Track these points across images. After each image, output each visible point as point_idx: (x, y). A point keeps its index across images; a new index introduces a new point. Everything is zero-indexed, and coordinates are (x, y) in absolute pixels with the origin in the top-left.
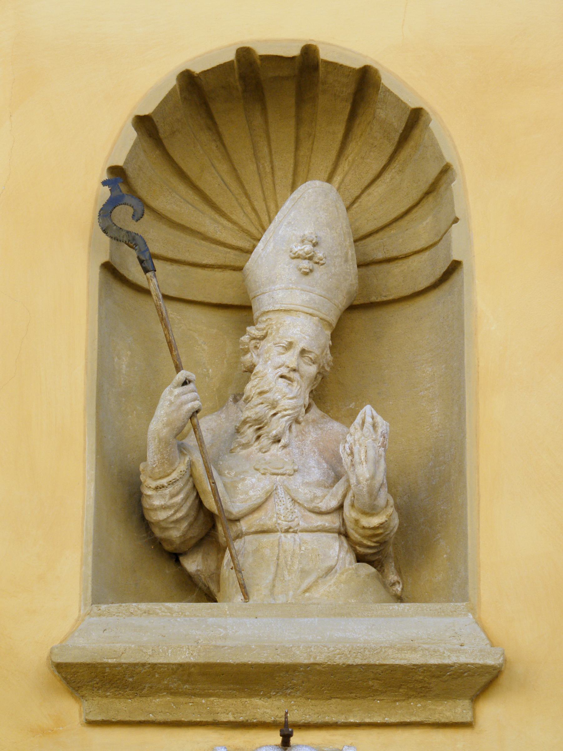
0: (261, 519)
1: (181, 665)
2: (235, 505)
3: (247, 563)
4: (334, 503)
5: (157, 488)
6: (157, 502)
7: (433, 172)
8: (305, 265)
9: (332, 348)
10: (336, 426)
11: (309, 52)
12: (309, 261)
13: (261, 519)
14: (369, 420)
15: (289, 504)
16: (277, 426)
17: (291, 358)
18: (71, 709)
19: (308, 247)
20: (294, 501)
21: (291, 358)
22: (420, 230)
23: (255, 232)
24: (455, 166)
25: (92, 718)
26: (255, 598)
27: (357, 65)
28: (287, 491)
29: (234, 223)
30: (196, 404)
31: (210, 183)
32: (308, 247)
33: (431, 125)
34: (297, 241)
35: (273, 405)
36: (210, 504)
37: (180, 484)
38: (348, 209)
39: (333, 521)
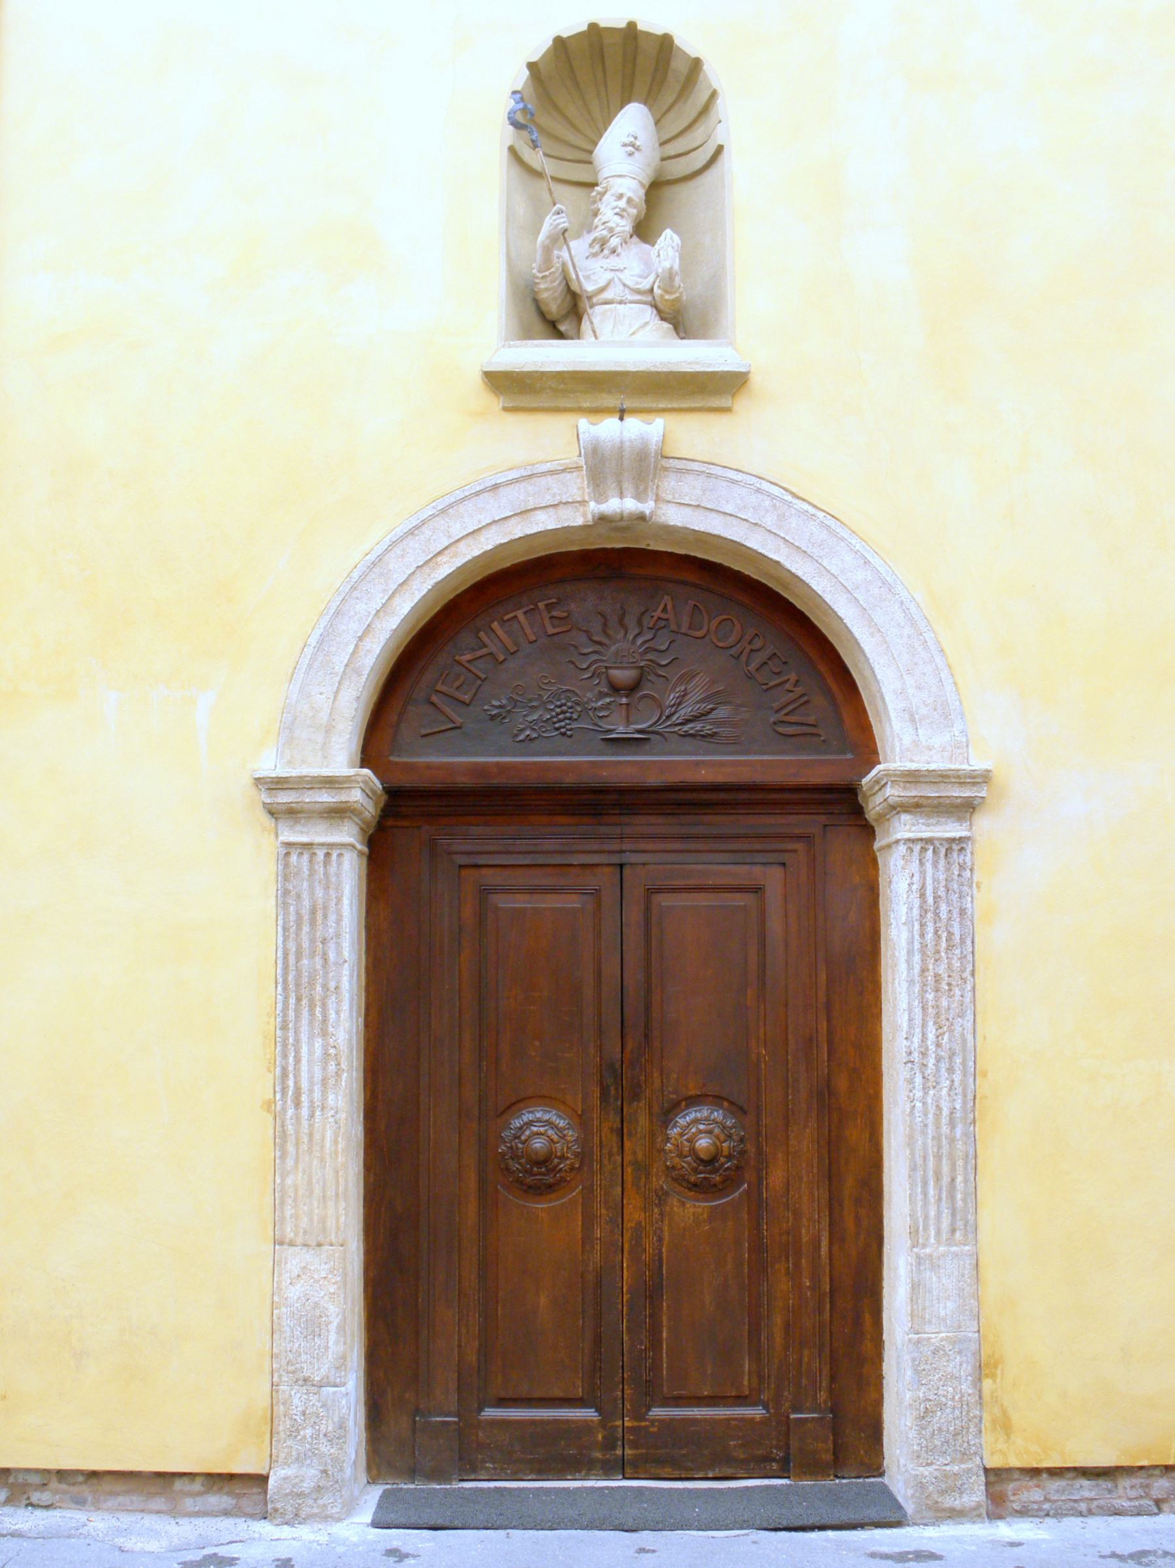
0: (607, 295)
1: (559, 372)
2: (589, 287)
3: (596, 321)
4: (648, 287)
5: (543, 277)
6: (542, 287)
7: (705, 96)
8: (630, 148)
9: (646, 201)
10: (648, 246)
11: (632, 25)
12: (633, 147)
13: (607, 295)
14: (669, 236)
15: (621, 287)
16: (614, 242)
17: (622, 203)
18: (496, 403)
19: (632, 139)
20: (624, 285)
21: (622, 203)
22: (698, 134)
23: (778, 1339)
24: (719, 91)
25: (548, 152)
26: (602, 339)
27: (694, 55)
28: (620, 279)
29: (585, 136)
30: (566, 225)
31: (572, 111)
32: (632, 139)
33: (704, 67)
34: (626, 141)
35: (611, 230)
36: (575, 287)
37: (557, 275)
38: (656, 123)
39: (650, 298)
